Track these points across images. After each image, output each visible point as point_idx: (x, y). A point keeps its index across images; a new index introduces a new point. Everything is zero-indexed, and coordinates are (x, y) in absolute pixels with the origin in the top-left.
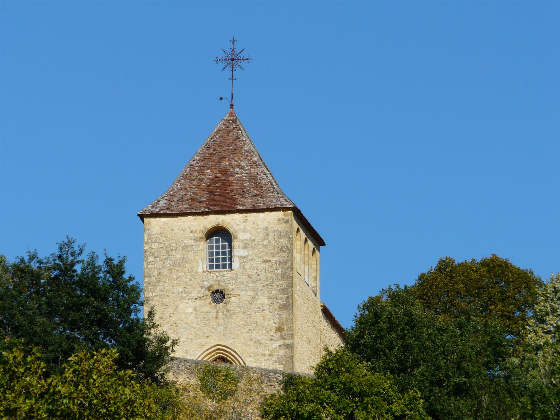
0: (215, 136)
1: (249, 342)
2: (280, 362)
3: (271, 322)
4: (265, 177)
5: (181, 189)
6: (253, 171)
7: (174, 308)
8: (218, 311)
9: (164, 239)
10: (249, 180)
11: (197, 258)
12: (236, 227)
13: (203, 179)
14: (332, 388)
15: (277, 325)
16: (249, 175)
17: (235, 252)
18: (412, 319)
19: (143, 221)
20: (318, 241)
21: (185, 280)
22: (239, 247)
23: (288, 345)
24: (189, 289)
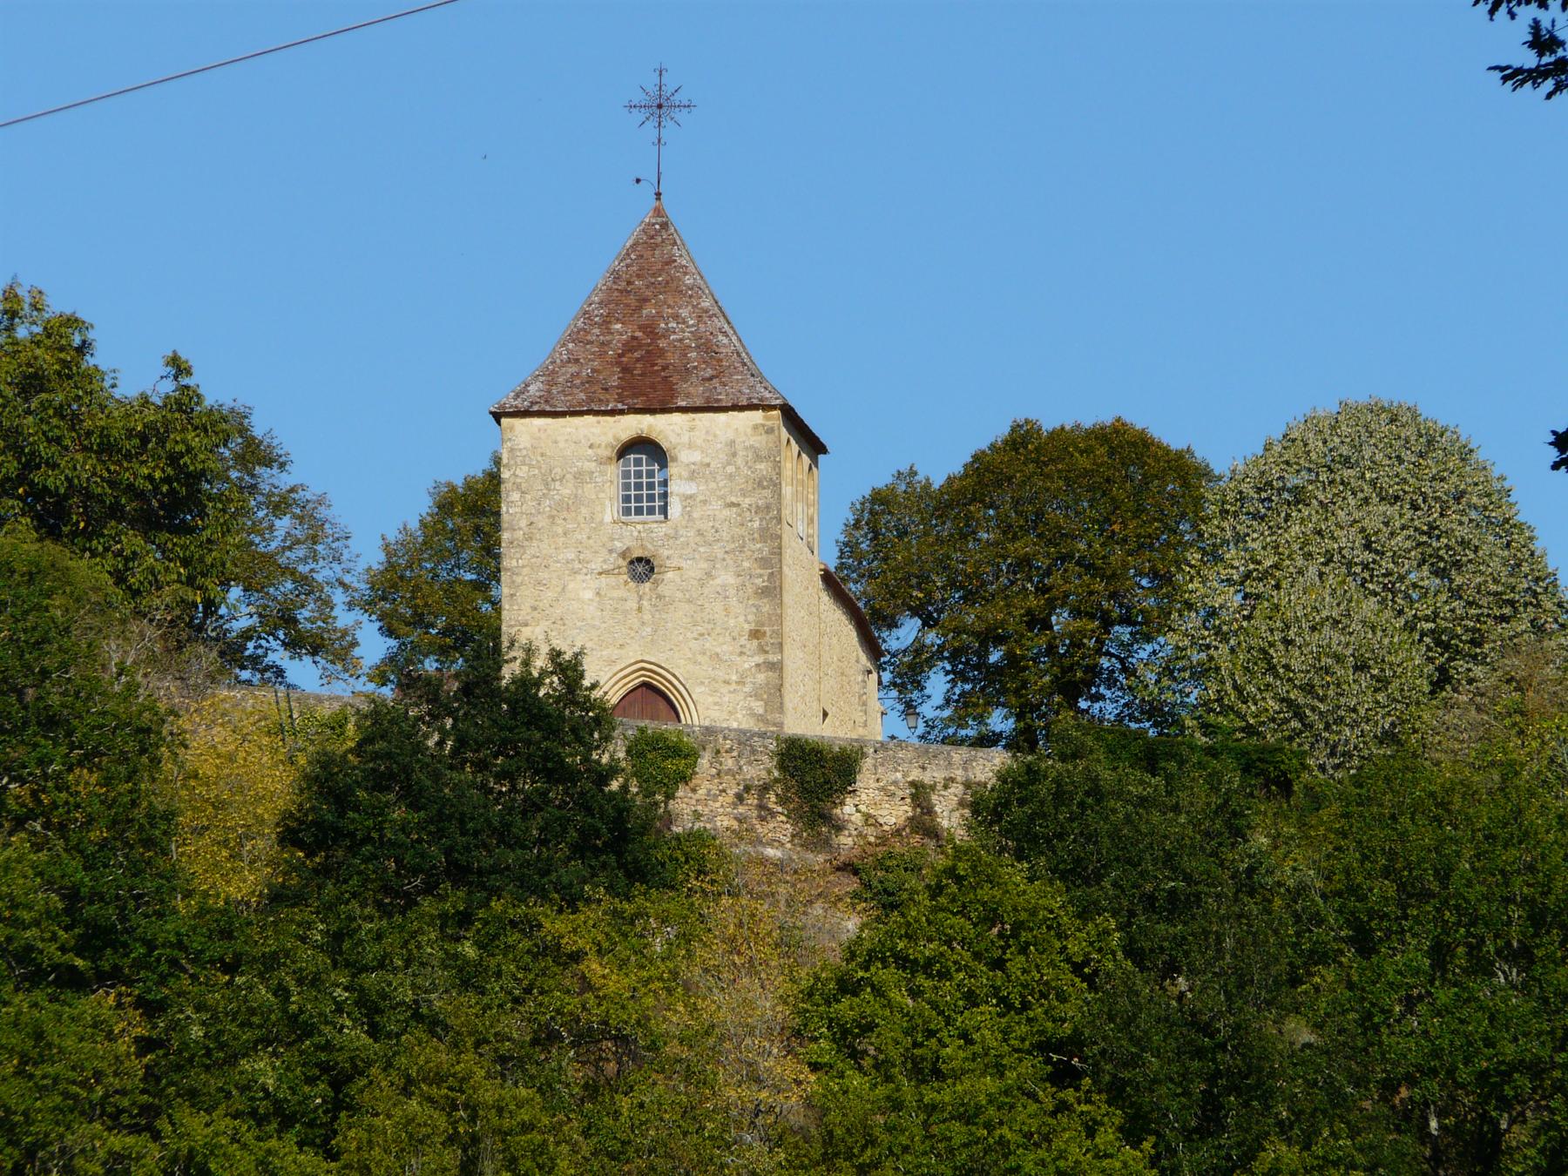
0: (628, 254)
1: (700, 658)
2: (757, 696)
3: (742, 620)
4: (725, 341)
5: (569, 361)
6: (702, 328)
7: (559, 589)
8: (641, 598)
9: (539, 458)
10: (698, 347)
11: (602, 495)
12: (674, 439)
13: (610, 342)
14: (962, 913)
15: (753, 626)
16: (697, 336)
17: (673, 487)
18: (1097, 786)
19: (499, 423)
20: (813, 445)
21: (579, 537)
22: (680, 477)
23: (773, 664)
24: (587, 555)
